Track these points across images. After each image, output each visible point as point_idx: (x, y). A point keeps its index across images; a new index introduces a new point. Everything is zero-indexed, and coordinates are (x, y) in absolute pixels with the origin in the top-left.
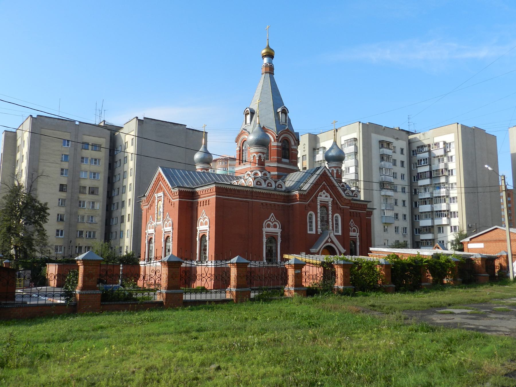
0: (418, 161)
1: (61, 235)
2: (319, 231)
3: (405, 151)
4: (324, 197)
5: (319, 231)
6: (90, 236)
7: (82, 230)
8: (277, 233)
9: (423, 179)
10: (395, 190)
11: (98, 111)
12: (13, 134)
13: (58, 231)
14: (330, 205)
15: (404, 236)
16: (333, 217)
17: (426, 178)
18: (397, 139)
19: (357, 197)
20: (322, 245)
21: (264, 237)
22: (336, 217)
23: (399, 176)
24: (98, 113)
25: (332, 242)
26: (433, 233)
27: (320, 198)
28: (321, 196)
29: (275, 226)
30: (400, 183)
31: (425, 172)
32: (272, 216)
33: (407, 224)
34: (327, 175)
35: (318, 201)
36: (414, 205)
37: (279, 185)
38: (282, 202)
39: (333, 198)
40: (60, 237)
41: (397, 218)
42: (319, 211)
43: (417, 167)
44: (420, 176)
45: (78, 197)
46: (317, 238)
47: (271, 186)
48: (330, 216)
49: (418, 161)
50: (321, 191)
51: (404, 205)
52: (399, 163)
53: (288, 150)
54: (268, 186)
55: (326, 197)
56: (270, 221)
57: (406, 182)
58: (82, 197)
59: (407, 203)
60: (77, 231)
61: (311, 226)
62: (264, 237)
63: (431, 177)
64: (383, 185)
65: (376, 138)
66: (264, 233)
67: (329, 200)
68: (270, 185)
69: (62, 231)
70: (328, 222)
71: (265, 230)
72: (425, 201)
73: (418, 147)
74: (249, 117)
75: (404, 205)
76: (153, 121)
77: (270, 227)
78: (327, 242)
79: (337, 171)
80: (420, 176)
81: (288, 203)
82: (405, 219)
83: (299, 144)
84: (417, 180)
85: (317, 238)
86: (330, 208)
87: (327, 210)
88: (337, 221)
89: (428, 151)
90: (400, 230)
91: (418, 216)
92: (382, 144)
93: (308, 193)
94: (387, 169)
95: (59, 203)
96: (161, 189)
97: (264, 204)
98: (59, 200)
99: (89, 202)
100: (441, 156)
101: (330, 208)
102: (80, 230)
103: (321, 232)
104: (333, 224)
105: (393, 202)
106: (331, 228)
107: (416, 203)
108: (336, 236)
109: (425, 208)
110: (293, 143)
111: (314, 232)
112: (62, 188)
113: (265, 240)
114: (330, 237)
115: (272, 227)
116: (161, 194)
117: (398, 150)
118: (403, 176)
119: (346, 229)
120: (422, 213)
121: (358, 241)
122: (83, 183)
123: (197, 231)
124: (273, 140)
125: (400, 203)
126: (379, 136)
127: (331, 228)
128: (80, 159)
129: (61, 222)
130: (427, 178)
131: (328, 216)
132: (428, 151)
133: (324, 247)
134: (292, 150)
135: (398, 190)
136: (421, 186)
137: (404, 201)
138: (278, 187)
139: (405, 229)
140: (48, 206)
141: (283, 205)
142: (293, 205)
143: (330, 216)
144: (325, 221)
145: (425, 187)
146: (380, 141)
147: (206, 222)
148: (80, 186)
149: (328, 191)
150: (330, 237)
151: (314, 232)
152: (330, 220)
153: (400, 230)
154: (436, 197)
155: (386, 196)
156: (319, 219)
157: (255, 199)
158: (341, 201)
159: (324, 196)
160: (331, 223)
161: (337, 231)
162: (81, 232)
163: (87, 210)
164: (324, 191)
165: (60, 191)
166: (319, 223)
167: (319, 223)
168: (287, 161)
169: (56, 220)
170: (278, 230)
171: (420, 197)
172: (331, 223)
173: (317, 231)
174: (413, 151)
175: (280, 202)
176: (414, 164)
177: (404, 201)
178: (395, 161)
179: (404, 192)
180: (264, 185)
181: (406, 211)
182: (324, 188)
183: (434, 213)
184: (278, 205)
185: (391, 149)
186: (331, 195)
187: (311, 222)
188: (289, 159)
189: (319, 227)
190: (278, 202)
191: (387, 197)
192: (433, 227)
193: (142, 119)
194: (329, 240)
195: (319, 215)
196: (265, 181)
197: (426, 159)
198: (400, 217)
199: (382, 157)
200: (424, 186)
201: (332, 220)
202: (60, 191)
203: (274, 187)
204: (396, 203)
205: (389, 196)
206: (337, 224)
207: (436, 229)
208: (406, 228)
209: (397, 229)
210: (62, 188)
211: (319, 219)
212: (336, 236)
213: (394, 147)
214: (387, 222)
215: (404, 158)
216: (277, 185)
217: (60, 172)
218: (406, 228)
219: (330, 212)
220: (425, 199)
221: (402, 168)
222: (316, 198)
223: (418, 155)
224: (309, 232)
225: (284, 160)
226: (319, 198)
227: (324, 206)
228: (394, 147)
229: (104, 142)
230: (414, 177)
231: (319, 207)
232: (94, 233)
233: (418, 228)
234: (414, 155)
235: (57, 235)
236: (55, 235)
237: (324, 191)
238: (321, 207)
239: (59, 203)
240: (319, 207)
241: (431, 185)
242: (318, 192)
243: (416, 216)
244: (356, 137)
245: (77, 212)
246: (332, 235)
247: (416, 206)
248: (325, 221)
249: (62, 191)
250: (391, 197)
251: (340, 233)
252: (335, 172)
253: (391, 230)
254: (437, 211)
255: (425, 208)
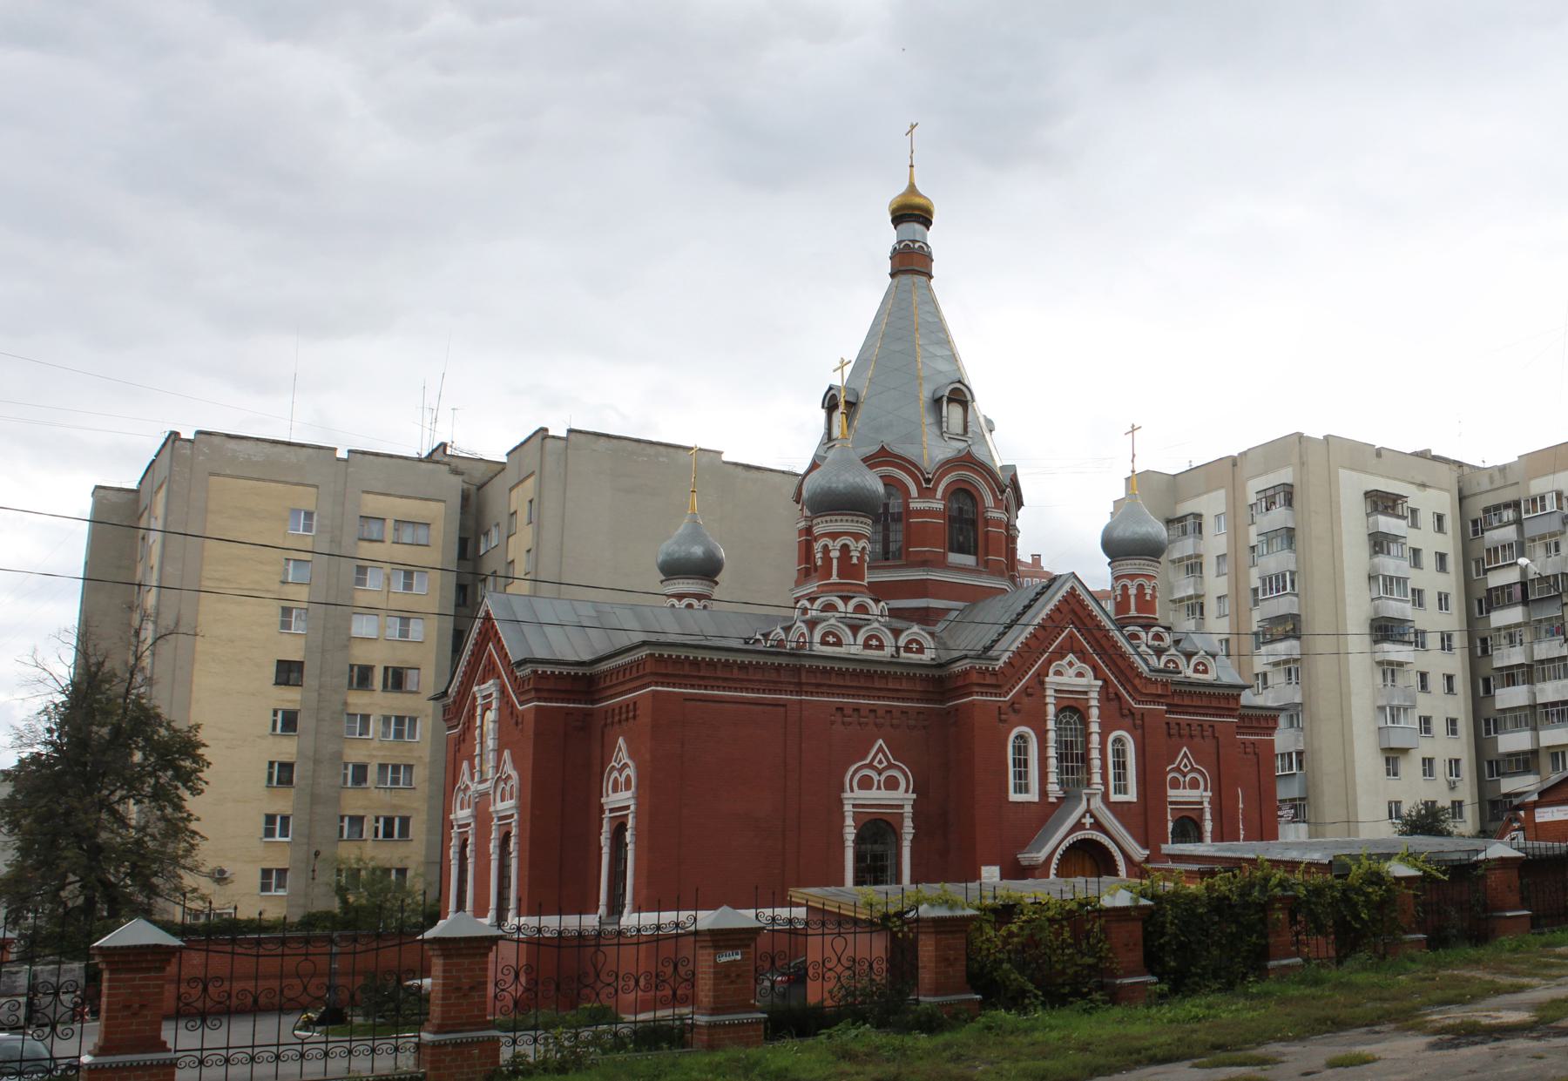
0: (1489, 550)
1: (284, 833)
2: (1054, 790)
3: (1448, 523)
4: (1071, 676)
5: (1054, 790)
6: (388, 834)
7: (361, 813)
8: (902, 806)
9: (1502, 607)
10: (1419, 640)
11: (427, 412)
12: (131, 496)
13: (270, 819)
14: (1094, 703)
15: (1452, 787)
16: (1103, 743)
17: (1510, 603)
18: (1423, 486)
19: (1205, 671)
20: (1057, 840)
21: (849, 821)
22: (1118, 740)
23: (1431, 599)
24: (428, 417)
25: (1098, 825)
26: (1538, 773)
27: (1058, 679)
28: (1058, 673)
29: (892, 784)
30: (1431, 620)
31: (1509, 586)
32: (880, 749)
33: (1461, 747)
34: (1081, 603)
35: (1050, 692)
36: (1483, 683)
37: (910, 642)
38: (918, 700)
39: (1105, 681)
40: (278, 838)
41: (1428, 731)
42: (1051, 725)
43: (1486, 571)
44: (1497, 598)
45: (345, 704)
46: (1046, 813)
47: (881, 647)
48: (1095, 739)
49: (1489, 550)
50: (1060, 654)
51: (1450, 689)
52: (1429, 560)
53: (974, 523)
54: (867, 646)
55: (1080, 675)
56: (870, 766)
57: (1452, 620)
58: (359, 701)
59: (1461, 684)
60: (342, 818)
61: (1021, 775)
62: (849, 821)
63: (1525, 601)
64: (1384, 629)
65: (1352, 486)
66: (848, 808)
67: (1090, 683)
68: (874, 642)
69: (285, 819)
70: (1085, 758)
71: (853, 797)
72: (1510, 676)
73: (1486, 510)
74: (838, 417)
75: (1450, 689)
76: (602, 440)
77: (869, 787)
78: (1079, 826)
79: (1141, 587)
80: (1497, 598)
81: (942, 702)
82: (1454, 732)
83: (1020, 504)
84: (1488, 612)
85: (1046, 813)
86: (1094, 712)
87: (1084, 720)
88: (1120, 753)
89: (1515, 522)
90: (1440, 768)
91: (1495, 721)
92: (1382, 502)
93: (1010, 664)
94: (1391, 578)
95: (275, 722)
96: (491, 671)
97: (848, 711)
98: (275, 713)
99: (386, 719)
100: (1552, 535)
101: (1094, 712)
102: (352, 813)
103: (1060, 794)
104: (1104, 767)
105: (1415, 680)
106: (1097, 778)
107: (1487, 681)
108: (1115, 808)
109: (1510, 697)
110: (989, 500)
111: (1033, 796)
112: (288, 672)
113: (850, 833)
114: (1088, 811)
115: (878, 787)
116: (490, 686)
117: (1426, 519)
118: (1443, 600)
119: (1151, 782)
120: (1503, 711)
121: (1208, 816)
122: (361, 656)
123: (602, 811)
124: (914, 491)
125: (1436, 683)
126: (1363, 476)
127: (1097, 778)
128: (354, 574)
129: (284, 790)
130: (1515, 604)
131: (1087, 741)
132: (1515, 522)
133: (1066, 843)
134: (987, 522)
135: (1429, 645)
136: (1499, 629)
137: (1450, 678)
138: (908, 649)
139: (1454, 764)
140: (202, 736)
141: (920, 712)
142: (957, 708)
143: (1095, 739)
144: (1074, 760)
145: (1511, 635)
146: (1366, 494)
147: (628, 778)
148: (352, 666)
149: (1083, 656)
150: (1088, 811)
151: (1033, 796)
152: (1095, 754)
153: (1440, 768)
154: (1542, 662)
155: (1390, 663)
156: (1052, 752)
157: (812, 694)
158: (1135, 687)
159: (1072, 672)
160: (1096, 763)
161: (1122, 789)
162: (357, 821)
163: (376, 743)
164: (1070, 657)
165: (277, 683)
166: (1053, 762)
167: (1053, 762)
168: (969, 560)
169: (265, 782)
170: (903, 797)
171: (1497, 664)
172: (1096, 763)
173: (1043, 793)
174: (1475, 522)
175: (912, 700)
176: (1477, 562)
177: (1450, 678)
178: (1416, 552)
179: (1450, 649)
180: (853, 647)
181: (1458, 705)
182: (1071, 647)
183: (1539, 710)
184: (904, 712)
185: (1404, 518)
186: (1095, 668)
187: (1022, 763)
188: (975, 554)
189: (1053, 778)
190: (903, 700)
191: (1390, 669)
192: (1535, 753)
193: (564, 434)
194: (1088, 821)
195: (1052, 736)
196: (855, 629)
197: (1510, 546)
198: (1439, 726)
199: (1379, 543)
200: (1508, 627)
201: (1103, 752)
202: (277, 683)
203: (889, 651)
204: (1424, 687)
205: (1400, 664)
206: (1121, 765)
207: (1545, 762)
208: (1457, 761)
209: (1428, 763)
210: (288, 672)
211: (1052, 752)
212: (1115, 808)
213: (1414, 511)
214: (1393, 745)
215: (1448, 543)
216: (902, 642)
217: (278, 619)
218: (1457, 761)
219: (1095, 728)
220: (1511, 667)
221: (1442, 576)
222: (1042, 683)
223: (1487, 534)
224: (1014, 797)
225: (955, 558)
226: (1051, 679)
227: (1073, 709)
228: (1414, 511)
229: (441, 517)
230: (1480, 602)
231: (1051, 709)
232: (405, 821)
233: (1494, 757)
234: (1475, 532)
235: (269, 833)
236: (262, 832)
237: (1070, 657)
238: (1060, 711)
239: (275, 722)
240: (1051, 709)
241: (1526, 624)
242: (1049, 662)
243: (1487, 722)
244: (1289, 481)
245: (339, 755)
246: (1097, 803)
247: (1488, 690)
248: (1074, 760)
249: (287, 683)
250: (1406, 668)
251: (1132, 796)
252: (1132, 591)
253: (1411, 768)
254: (1545, 705)
255: (1510, 697)
